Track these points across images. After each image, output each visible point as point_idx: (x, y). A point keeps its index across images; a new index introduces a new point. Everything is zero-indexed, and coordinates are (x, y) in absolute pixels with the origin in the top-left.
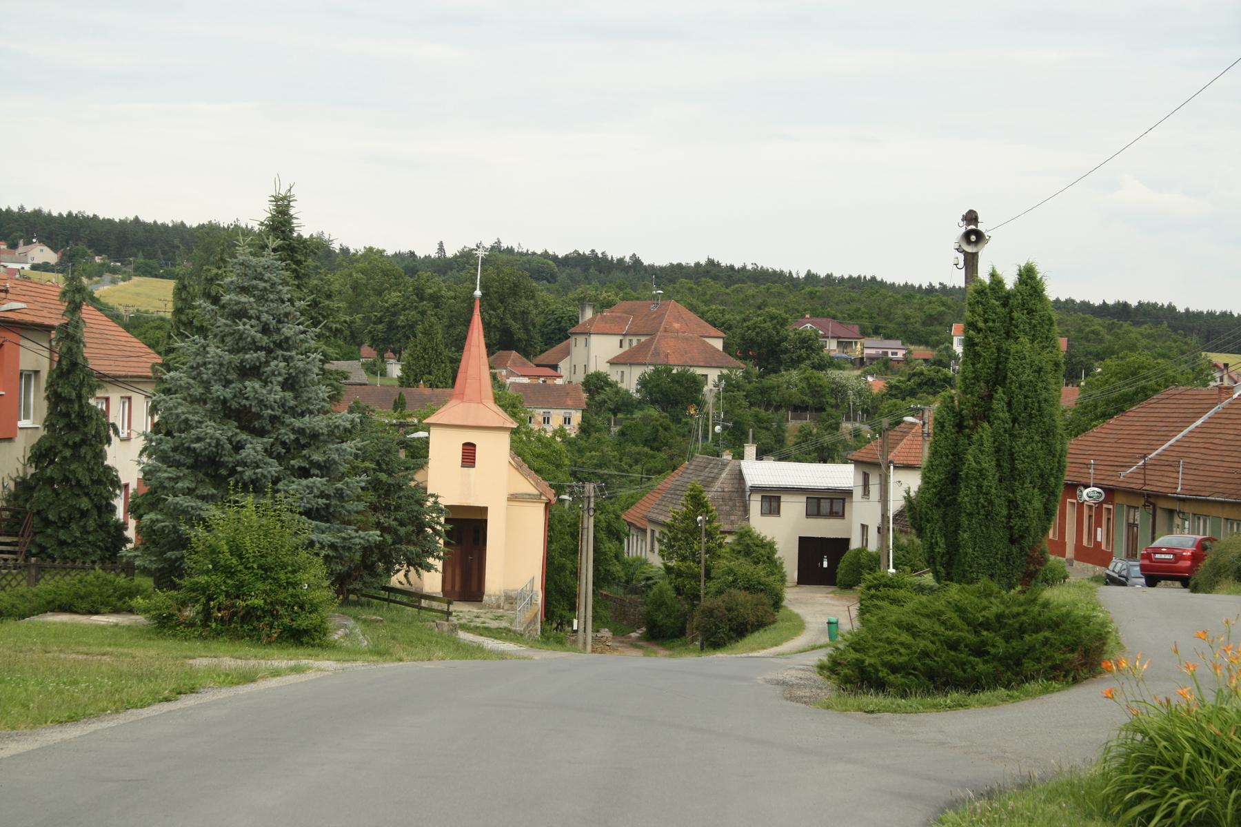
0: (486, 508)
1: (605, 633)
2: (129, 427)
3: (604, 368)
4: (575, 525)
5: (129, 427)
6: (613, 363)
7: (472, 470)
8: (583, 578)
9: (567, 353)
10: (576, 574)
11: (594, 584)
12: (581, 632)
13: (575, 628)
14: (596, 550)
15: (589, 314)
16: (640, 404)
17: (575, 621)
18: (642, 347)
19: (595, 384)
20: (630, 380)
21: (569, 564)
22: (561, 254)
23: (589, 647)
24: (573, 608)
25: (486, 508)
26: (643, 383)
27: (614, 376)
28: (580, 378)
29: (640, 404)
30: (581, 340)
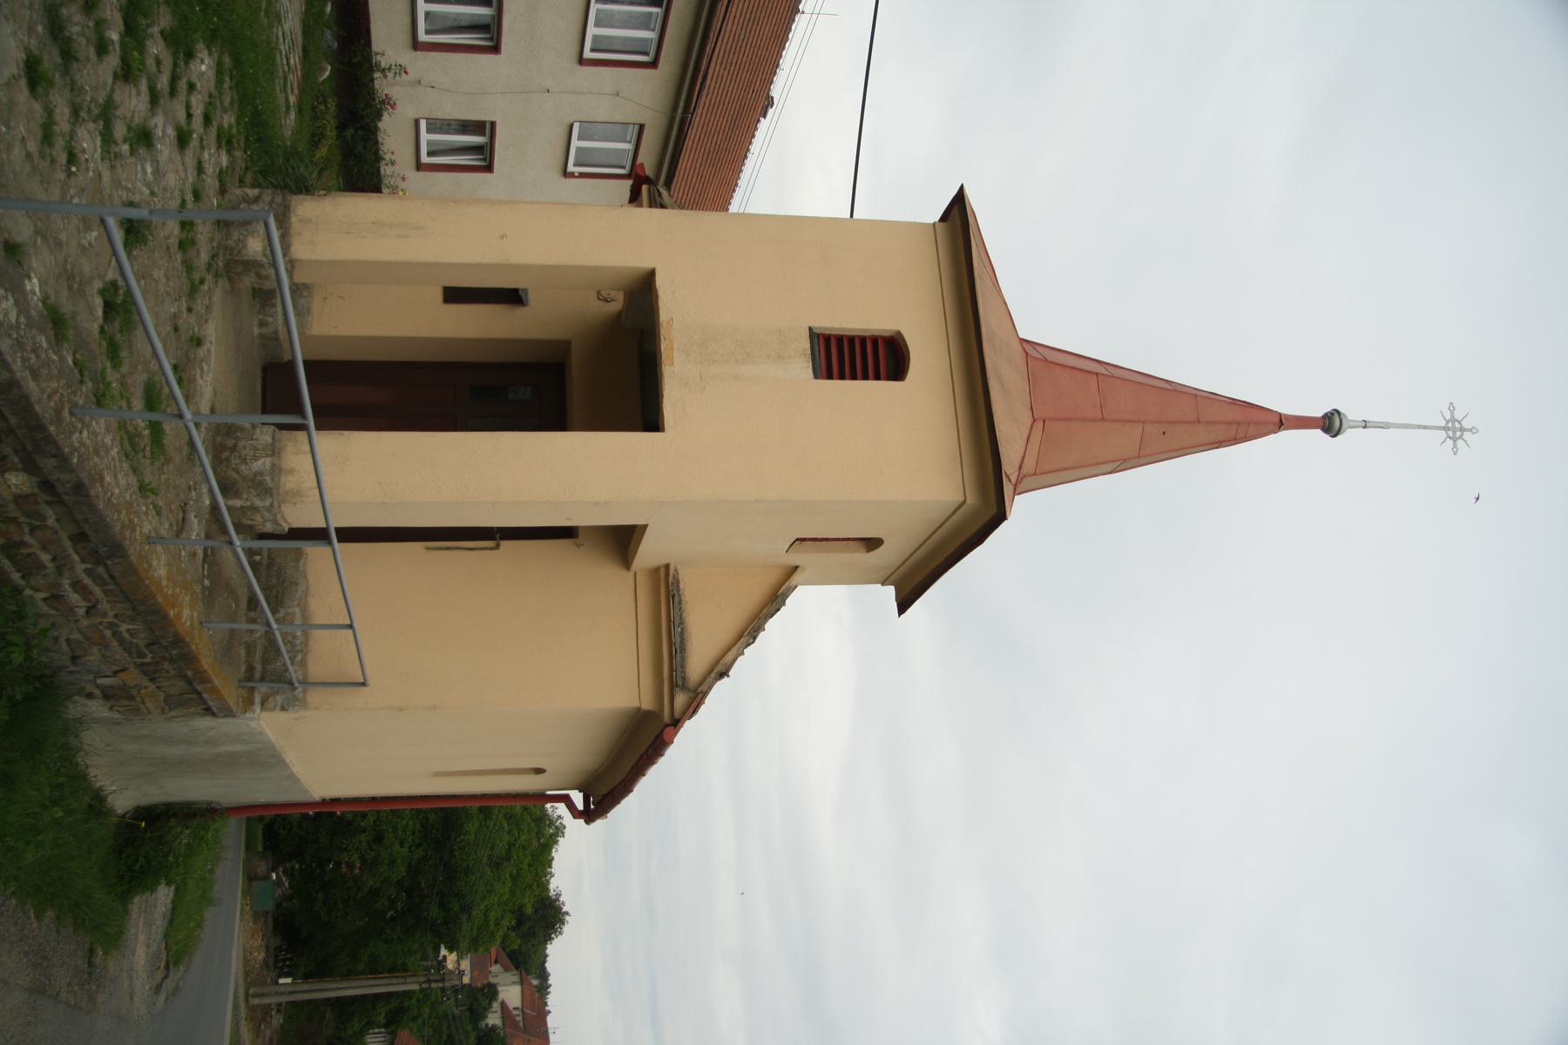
0: (651, 421)
1: (277, 1020)
2: (582, 175)
3: (502, 996)
4: (406, 970)
5: (582, 175)
6: (503, 1004)
7: (804, 368)
8: (345, 984)
9: (506, 970)
10: (349, 975)
11: (337, 999)
12: (277, 988)
13: (281, 981)
14: (378, 996)
15: (535, 982)
16: (476, 1027)
17: (289, 980)
18: (516, 1024)
19: (491, 992)
20: (493, 1019)
21: (361, 967)
22: (547, 965)
23: (256, 1001)
24: (307, 977)
25: (651, 421)
26: (494, 1028)
27: (496, 1006)
28: (492, 980)
29: (476, 1027)
30: (517, 978)
